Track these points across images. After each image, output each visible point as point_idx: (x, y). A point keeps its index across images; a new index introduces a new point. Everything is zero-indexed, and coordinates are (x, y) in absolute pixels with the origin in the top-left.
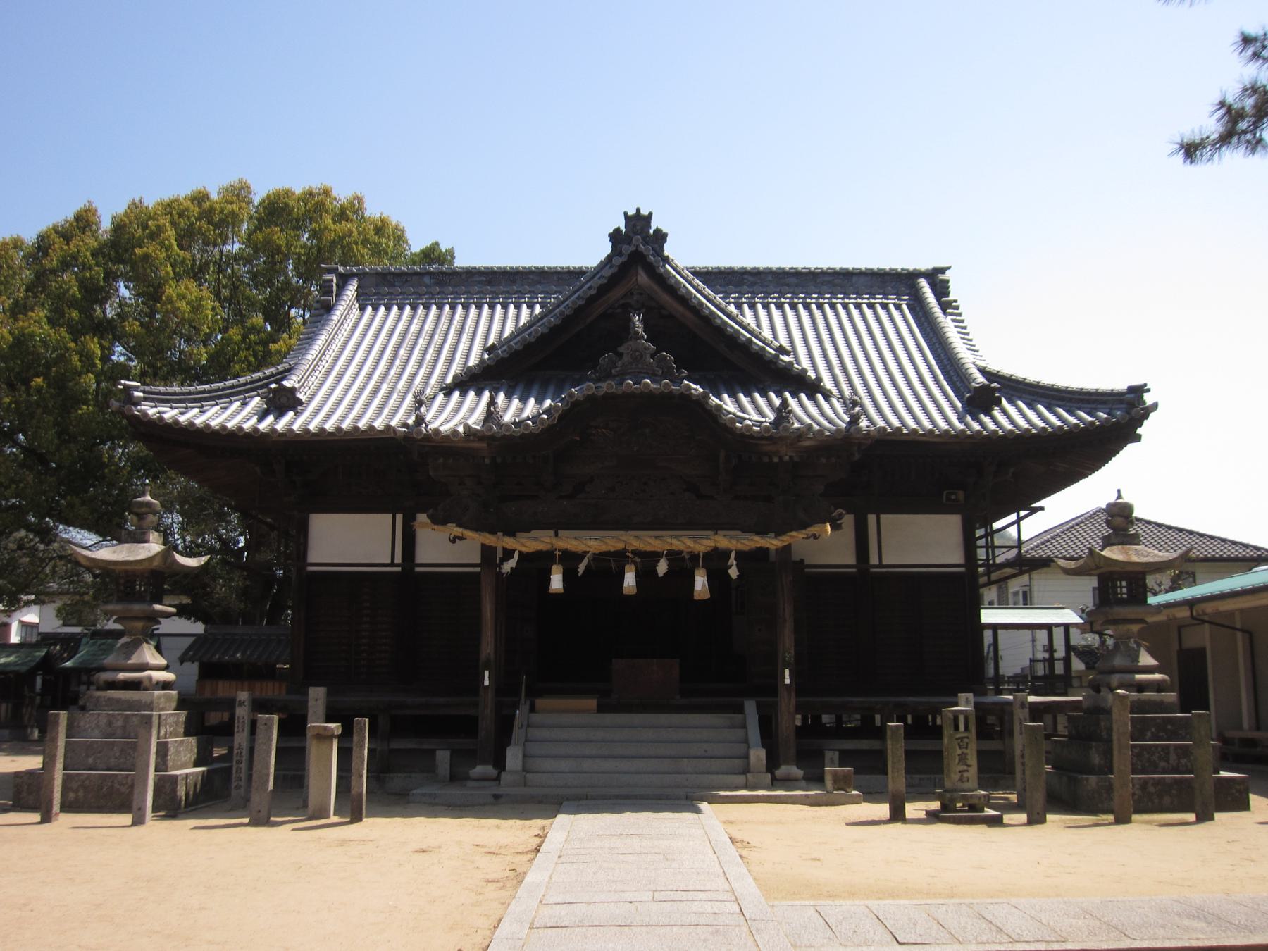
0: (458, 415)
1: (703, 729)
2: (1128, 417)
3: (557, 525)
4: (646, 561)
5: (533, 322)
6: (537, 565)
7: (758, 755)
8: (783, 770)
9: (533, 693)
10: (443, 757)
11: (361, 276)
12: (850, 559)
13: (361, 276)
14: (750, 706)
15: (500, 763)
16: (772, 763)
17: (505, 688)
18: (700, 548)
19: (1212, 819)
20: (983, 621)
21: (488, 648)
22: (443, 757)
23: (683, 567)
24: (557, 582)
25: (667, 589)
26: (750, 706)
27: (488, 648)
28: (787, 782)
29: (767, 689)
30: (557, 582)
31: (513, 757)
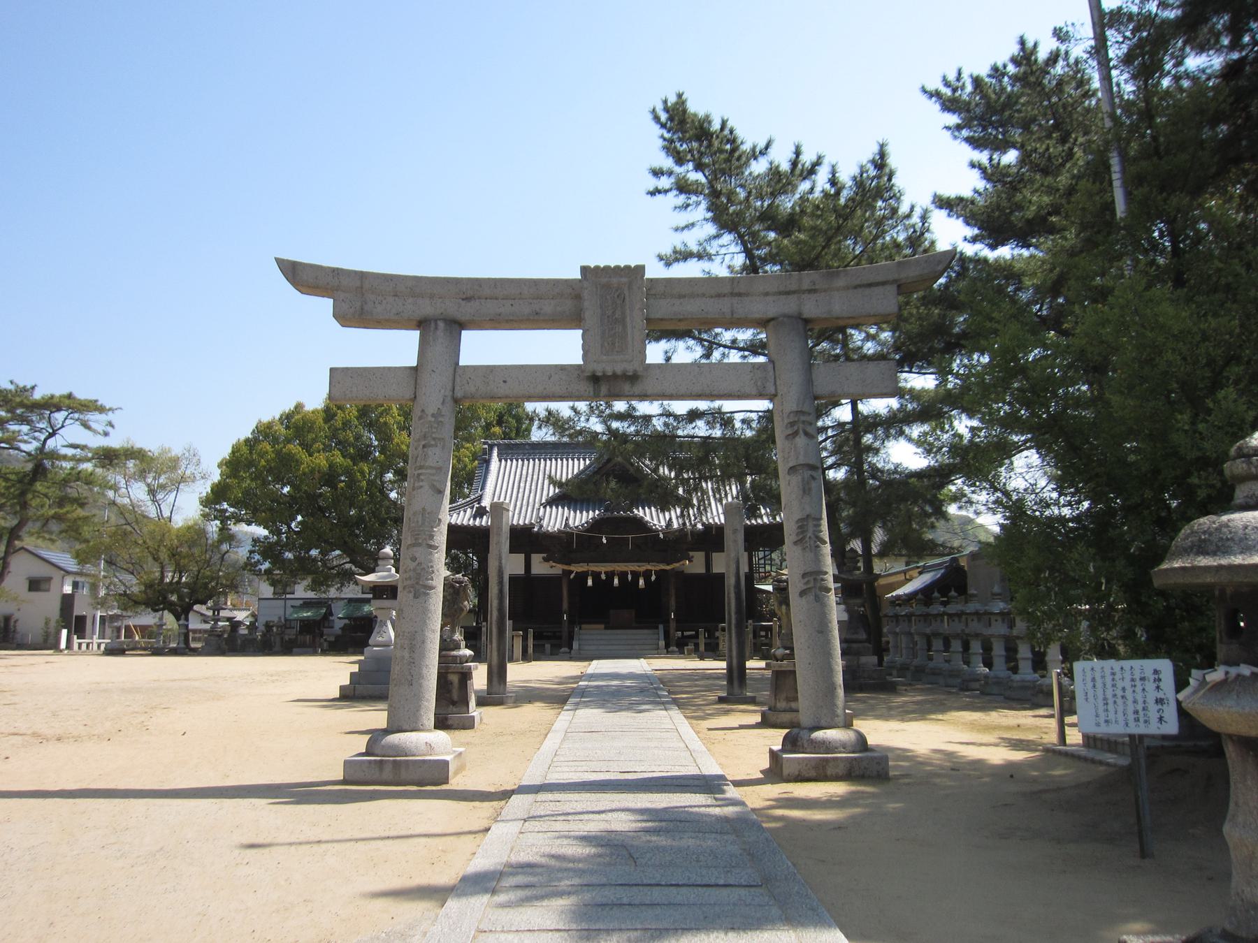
0: (555, 520)
1: (643, 634)
2: (942, 390)
3: (588, 561)
4: (623, 575)
5: (587, 468)
6: (582, 577)
7: (662, 643)
8: (671, 649)
9: (580, 623)
10: (548, 646)
11: (499, 445)
12: (703, 571)
13: (499, 445)
14: (661, 627)
15: (571, 647)
16: (667, 646)
17: (572, 622)
18: (641, 570)
19: (585, 270)
20: (533, 556)
21: (565, 606)
22: (548, 646)
23: (636, 575)
24: (590, 583)
25: (628, 585)
26: (661, 627)
27: (565, 606)
28: (672, 653)
29: (666, 622)
30: (590, 583)
31: (575, 645)
